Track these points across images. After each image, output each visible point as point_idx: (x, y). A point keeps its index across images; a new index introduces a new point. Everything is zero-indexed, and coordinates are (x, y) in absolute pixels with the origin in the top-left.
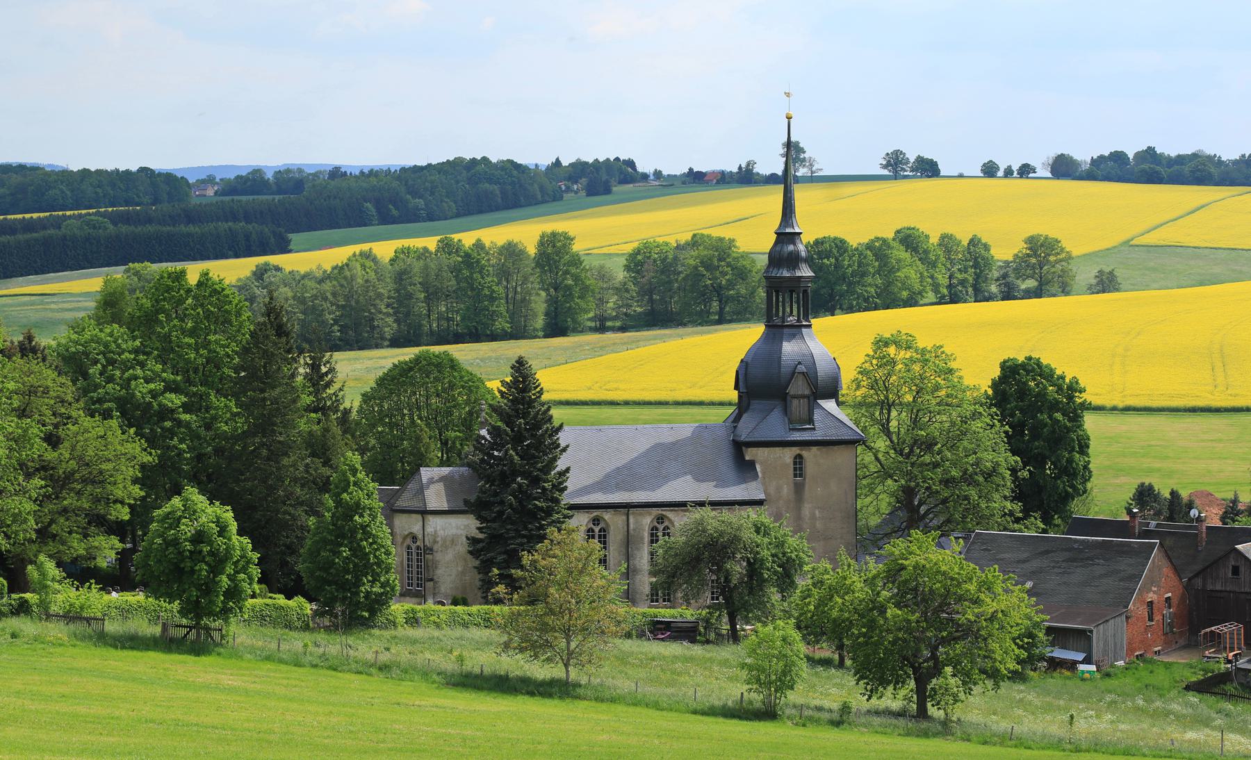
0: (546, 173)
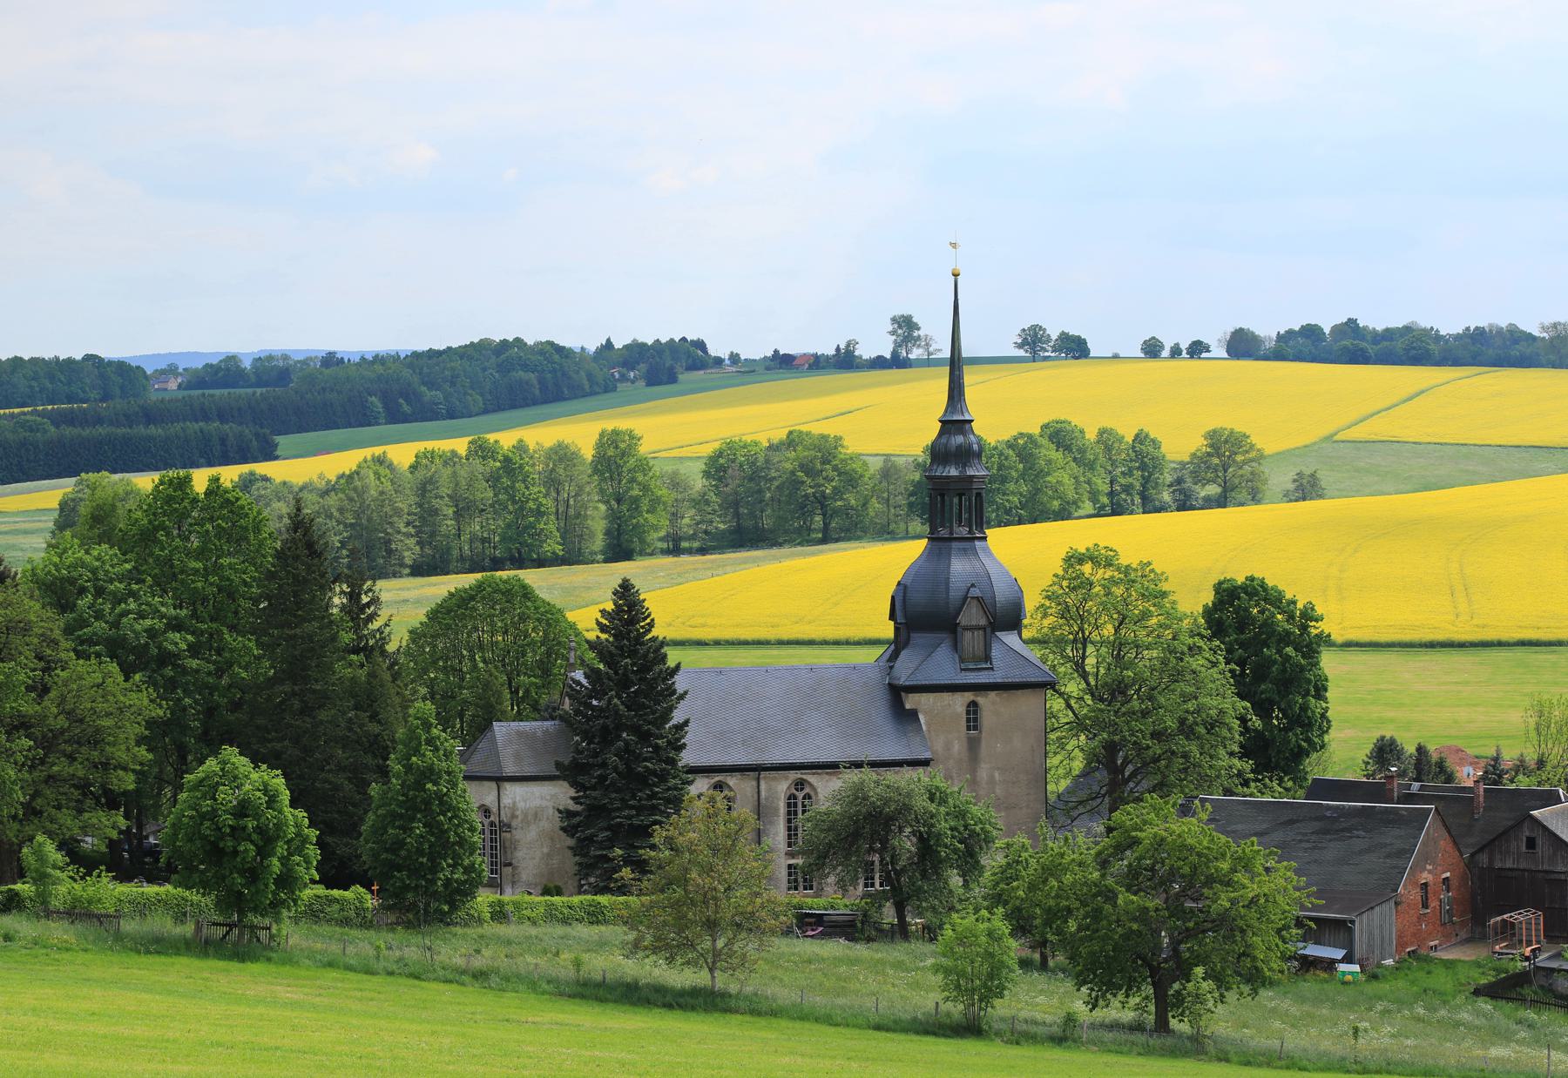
0: (595, 358)
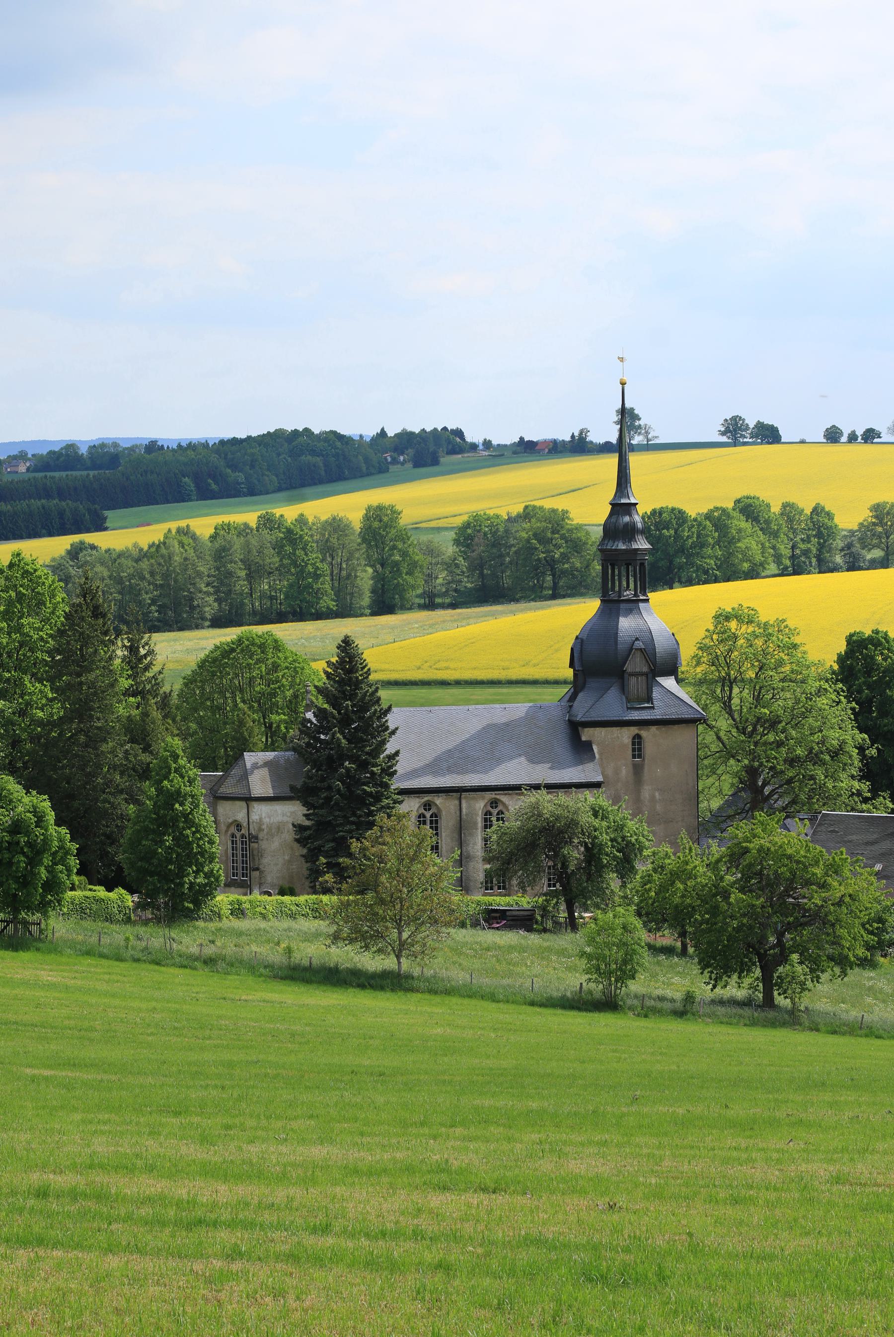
0: (371, 444)
